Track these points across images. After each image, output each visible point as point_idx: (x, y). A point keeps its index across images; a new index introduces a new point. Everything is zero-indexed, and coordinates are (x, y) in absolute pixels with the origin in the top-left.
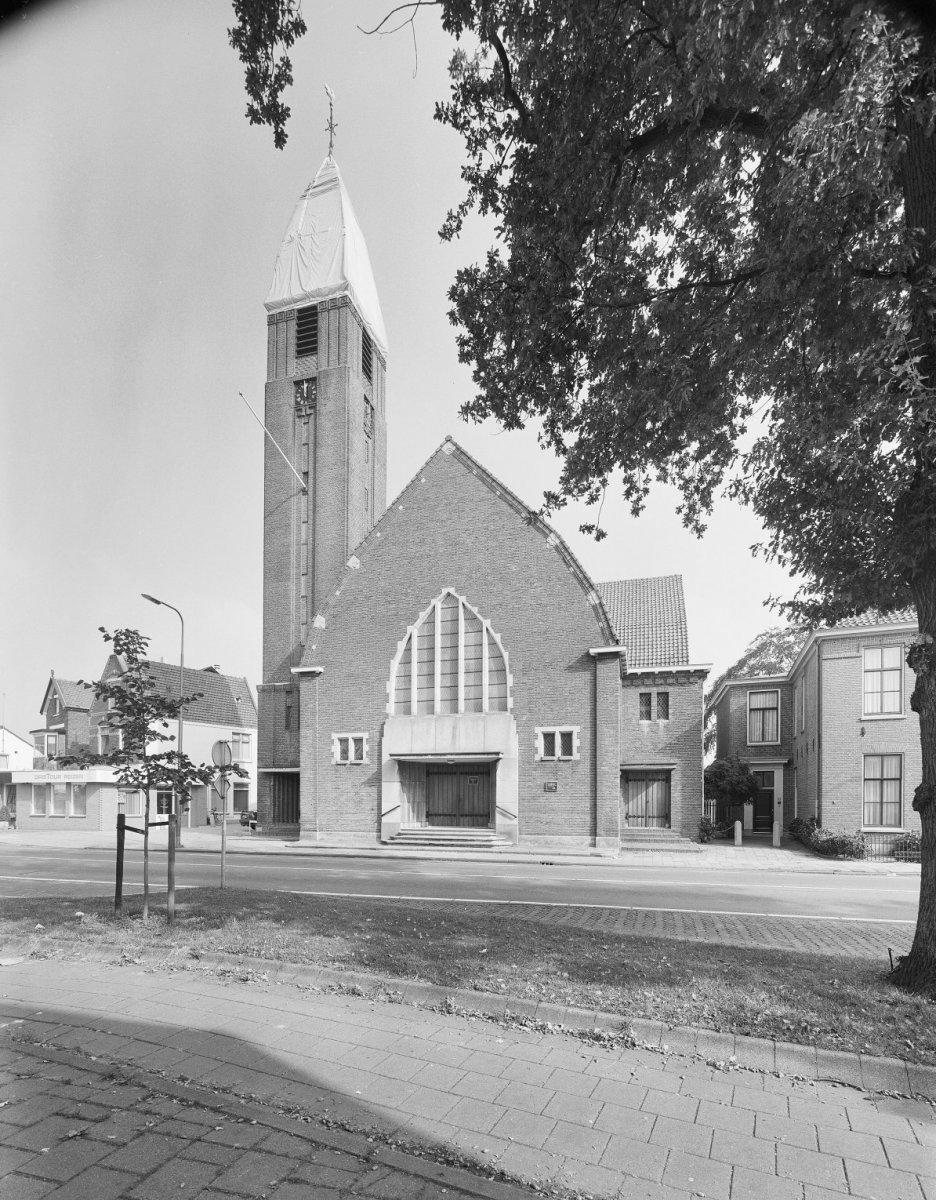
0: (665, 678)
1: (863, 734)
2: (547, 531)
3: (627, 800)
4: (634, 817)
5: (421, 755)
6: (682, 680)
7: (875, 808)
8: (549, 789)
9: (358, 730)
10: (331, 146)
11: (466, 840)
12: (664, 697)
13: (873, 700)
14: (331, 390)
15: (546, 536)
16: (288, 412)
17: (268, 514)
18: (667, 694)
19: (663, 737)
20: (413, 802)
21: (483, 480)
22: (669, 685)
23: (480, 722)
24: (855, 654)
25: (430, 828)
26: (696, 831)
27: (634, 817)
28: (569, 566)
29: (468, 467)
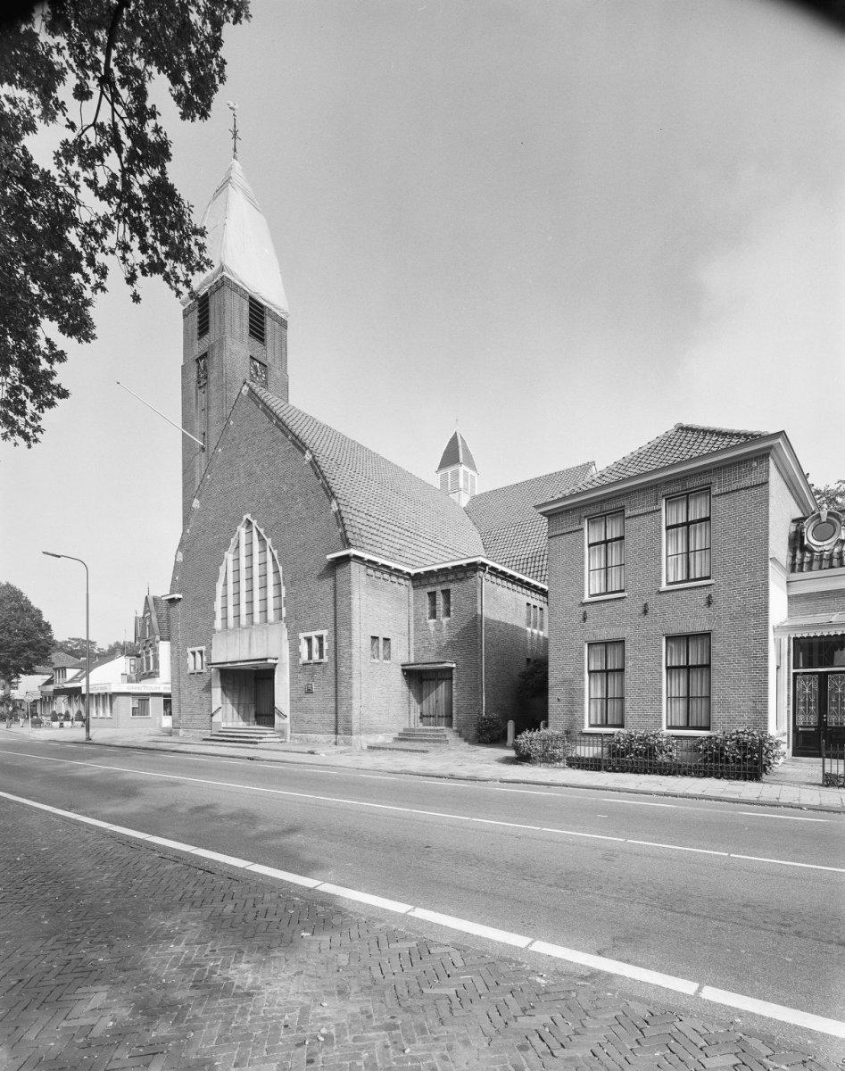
0: (446, 575)
1: (585, 619)
2: (304, 448)
3: (420, 701)
4: (427, 716)
5: (236, 662)
6: (461, 575)
7: (602, 704)
8: (309, 691)
9: (199, 645)
10: (235, 150)
11: (247, 737)
12: (446, 593)
13: (695, 574)
14: (215, 359)
15: (304, 453)
16: (193, 385)
17: (184, 472)
18: (449, 591)
19: (446, 635)
20: (238, 706)
21: (266, 413)
22: (451, 581)
23: (265, 631)
24: (577, 527)
25: (256, 727)
26: (473, 732)
27: (427, 716)
28: (319, 478)
29: (256, 403)
